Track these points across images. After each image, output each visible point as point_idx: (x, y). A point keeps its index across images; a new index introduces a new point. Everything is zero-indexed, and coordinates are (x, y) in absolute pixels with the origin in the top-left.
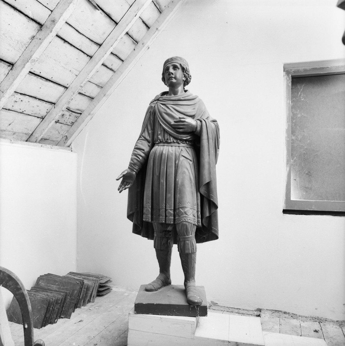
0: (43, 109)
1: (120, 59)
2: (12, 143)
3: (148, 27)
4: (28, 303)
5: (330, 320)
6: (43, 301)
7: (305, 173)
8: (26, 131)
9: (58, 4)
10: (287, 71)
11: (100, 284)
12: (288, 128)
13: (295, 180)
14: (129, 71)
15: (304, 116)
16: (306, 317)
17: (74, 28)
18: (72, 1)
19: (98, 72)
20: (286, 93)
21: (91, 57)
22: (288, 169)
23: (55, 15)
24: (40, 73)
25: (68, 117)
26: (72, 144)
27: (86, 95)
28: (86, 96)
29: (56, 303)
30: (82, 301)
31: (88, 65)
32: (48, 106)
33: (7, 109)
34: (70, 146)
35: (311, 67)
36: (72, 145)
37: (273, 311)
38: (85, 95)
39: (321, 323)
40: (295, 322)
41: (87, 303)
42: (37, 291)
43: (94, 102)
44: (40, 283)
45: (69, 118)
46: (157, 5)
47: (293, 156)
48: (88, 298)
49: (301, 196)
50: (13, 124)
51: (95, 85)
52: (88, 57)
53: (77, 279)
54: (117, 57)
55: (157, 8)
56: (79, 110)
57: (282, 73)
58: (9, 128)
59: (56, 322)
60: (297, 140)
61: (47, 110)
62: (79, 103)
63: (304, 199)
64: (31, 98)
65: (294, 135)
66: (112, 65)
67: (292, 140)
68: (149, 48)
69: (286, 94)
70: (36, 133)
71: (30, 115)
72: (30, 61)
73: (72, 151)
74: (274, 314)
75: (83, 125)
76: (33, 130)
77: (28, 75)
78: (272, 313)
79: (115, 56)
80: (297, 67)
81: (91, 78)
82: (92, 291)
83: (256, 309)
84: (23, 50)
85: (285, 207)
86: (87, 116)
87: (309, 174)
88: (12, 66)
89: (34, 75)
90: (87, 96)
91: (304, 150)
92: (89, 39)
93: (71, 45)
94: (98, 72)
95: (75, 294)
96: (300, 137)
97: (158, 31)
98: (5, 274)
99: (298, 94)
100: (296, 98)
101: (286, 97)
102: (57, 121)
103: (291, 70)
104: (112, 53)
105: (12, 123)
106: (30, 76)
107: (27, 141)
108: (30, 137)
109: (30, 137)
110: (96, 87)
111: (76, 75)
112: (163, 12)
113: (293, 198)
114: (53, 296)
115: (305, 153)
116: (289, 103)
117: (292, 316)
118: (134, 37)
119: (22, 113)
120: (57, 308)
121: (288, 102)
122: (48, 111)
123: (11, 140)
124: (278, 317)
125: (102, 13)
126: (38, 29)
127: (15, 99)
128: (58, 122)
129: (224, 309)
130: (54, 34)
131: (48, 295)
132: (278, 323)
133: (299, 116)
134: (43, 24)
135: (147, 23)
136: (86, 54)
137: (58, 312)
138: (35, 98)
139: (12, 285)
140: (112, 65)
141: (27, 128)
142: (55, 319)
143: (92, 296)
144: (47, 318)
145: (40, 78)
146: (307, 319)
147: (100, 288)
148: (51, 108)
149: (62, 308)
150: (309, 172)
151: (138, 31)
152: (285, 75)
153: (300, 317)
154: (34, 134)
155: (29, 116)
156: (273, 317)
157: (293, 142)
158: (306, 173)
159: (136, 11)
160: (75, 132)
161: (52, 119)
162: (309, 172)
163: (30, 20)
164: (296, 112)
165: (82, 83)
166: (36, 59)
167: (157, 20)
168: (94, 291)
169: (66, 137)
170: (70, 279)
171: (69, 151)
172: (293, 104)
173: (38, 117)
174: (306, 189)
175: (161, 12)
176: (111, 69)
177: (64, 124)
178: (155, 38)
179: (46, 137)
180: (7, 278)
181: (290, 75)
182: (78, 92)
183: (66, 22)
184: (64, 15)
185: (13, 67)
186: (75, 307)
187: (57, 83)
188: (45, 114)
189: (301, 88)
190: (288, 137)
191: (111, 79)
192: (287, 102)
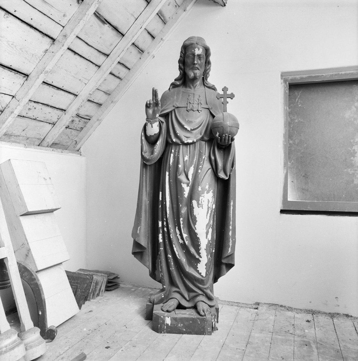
0: (54, 115)
1: (126, 67)
2: (26, 147)
3: (153, 37)
5: (323, 313)
7: (301, 175)
9: (69, 20)
10: (285, 79)
11: (108, 280)
12: (285, 133)
13: (293, 182)
16: (301, 310)
17: (84, 41)
18: (82, 18)
20: (284, 100)
21: (99, 67)
22: (285, 172)
23: (67, 30)
24: (52, 82)
25: (77, 122)
27: (95, 101)
28: (94, 102)
30: (92, 294)
32: (59, 112)
33: (21, 116)
34: (79, 150)
37: (270, 305)
40: (289, 314)
41: (96, 296)
43: (102, 108)
45: (78, 123)
46: (162, 17)
47: (291, 159)
48: (97, 292)
49: (298, 197)
50: (27, 129)
51: (103, 93)
53: (86, 274)
54: (124, 65)
55: (162, 19)
58: (23, 134)
62: (88, 110)
63: (301, 200)
64: (43, 106)
65: (292, 140)
66: (119, 73)
67: (290, 144)
69: (283, 101)
70: (47, 138)
71: (42, 121)
72: (43, 72)
74: (271, 307)
76: (44, 136)
77: (42, 85)
79: (122, 65)
81: (100, 86)
82: (101, 286)
83: (254, 303)
84: (37, 62)
87: (306, 176)
88: (27, 77)
90: (95, 103)
91: (301, 154)
92: (97, 50)
93: (81, 56)
95: (85, 287)
96: (297, 141)
97: (163, 41)
98: (21, 266)
100: (293, 104)
102: (67, 127)
104: (119, 62)
105: (26, 128)
107: (39, 145)
108: (42, 142)
109: (42, 142)
112: (167, 23)
116: (287, 109)
118: (140, 47)
121: (286, 108)
122: (59, 117)
123: (25, 145)
125: (110, 26)
126: (51, 44)
127: (29, 107)
129: (224, 303)
130: (65, 47)
133: (296, 122)
134: (55, 38)
135: (152, 34)
136: (95, 64)
138: (48, 105)
139: (28, 276)
140: (119, 73)
141: (39, 134)
143: (101, 291)
145: (52, 87)
147: (108, 283)
150: (306, 174)
151: (144, 41)
154: (45, 139)
155: (41, 122)
157: (291, 146)
158: (303, 175)
159: (141, 24)
161: (63, 125)
162: (306, 174)
163: (44, 36)
164: (293, 118)
165: (91, 91)
166: (49, 71)
167: (161, 31)
168: (102, 286)
170: (80, 274)
171: (78, 155)
172: (290, 110)
173: (50, 123)
174: (303, 190)
175: (165, 23)
176: (118, 78)
177: (74, 129)
178: (160, 48)
179: (57, 142)
180: (23, 270)
181: (288, 83)
182: (87, 99)
183: (77, 37)
184: (75, 30)
185: (28, 77)
186: (85, 300)
187: (67, 91)
189: (298, 93)
192: (285, 108)
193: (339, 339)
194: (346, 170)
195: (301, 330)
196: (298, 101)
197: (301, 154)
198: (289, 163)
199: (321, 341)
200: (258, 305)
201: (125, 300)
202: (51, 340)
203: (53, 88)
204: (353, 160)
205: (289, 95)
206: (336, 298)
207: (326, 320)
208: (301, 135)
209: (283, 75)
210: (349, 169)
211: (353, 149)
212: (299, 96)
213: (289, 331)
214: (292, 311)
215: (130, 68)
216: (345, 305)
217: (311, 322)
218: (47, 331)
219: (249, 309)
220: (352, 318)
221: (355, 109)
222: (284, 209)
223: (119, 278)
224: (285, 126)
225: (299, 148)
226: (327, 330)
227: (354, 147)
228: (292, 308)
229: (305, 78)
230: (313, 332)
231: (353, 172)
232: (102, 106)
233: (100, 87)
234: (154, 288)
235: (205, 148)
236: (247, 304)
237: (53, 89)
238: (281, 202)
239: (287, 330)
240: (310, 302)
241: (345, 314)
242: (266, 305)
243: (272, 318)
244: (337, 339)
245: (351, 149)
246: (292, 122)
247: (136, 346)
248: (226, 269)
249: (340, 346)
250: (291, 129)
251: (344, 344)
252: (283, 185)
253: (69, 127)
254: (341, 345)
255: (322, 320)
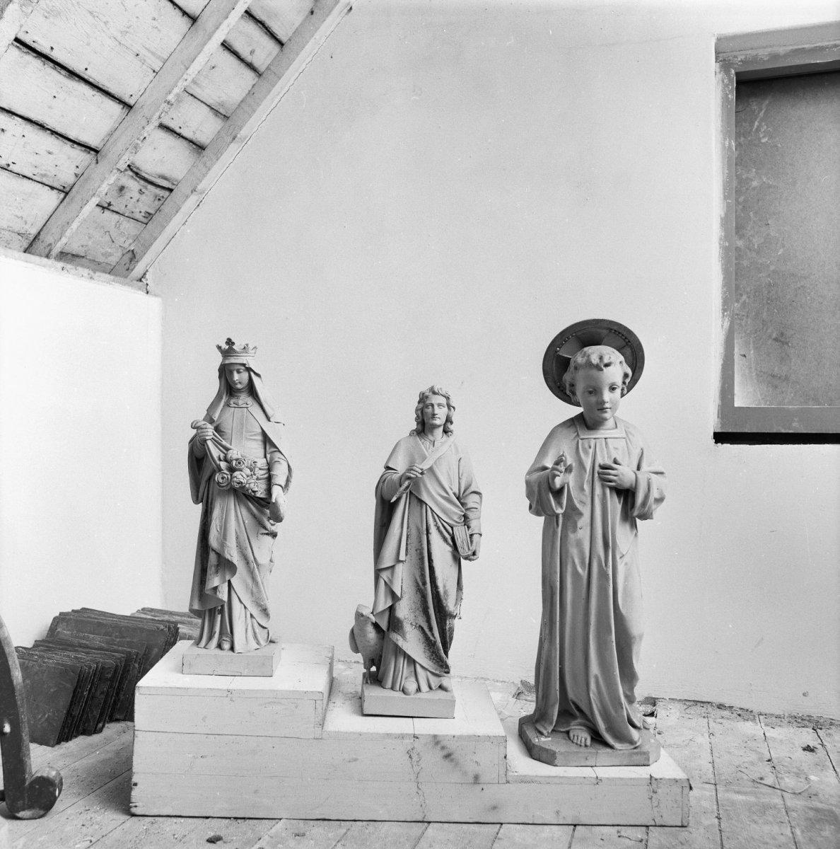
1: (273, 36)
4: (10, 663)
6: (64, 671)
7: (770, 336)
8: (18, 226)
10: (724, 60)
13: (745, 356)
14: (297, 74)
15: (769, 184)
19: (213, 67)
20: (722, 121)
22: (727, 324)
24: (52, 48)
25: (136, 195)
26: (148, 273)
29: (100, 679)
31: (185, 41)
35: (791, 48)
36: (147, 276)
38: (179, 135)
39: (818, 730)
40: (748, 728)
42: (49, 649)
43: (205, 157)
44: (59, 630)
45: (139, 199)
51: (208, 109)
52: (186, 19)
53: (158, 620)
54: (266, 28)
56: (166, 178)
57: (713, 65)
59: (101, 731)
60: (750, 250)
61: (77, 167)
65: (741, 237)
66: (252, 52)
67: (738, 249)
68: (351, 8)
70: (48, 233)
71: (29, 179)
73: (147, 293)
75: (178, 219)
78: (685, 707)
79: (261, 26)
80: (752, 49)
85: (720, 426)
86: (187, 197)
89: (35, 55)
94: (213, 67)
95: (153, 656)
96: (756, 241)
99: (753, 126)
100: (745, 137)
101: (722, 132)
102: (106, 205)
103: (735, 57)
106: (23, 55)
110: (211, 115)
111: (154, 71)
113: (738, 403)
114: (88, 660)
115: (770, 285)
117: (739, 715)
119: (6, 169)
120: (102, 693)
122: (79, 171)
124: (704, 717)
128: (109, 209)
131: (76, 658)
132: (704, 730)
136: (180, 8)
137: (105, 702)
138: (42, 127)
140: (252, 52)
142: (99, 722)
144: (74, 717)
145: (52, 65)
146: (781, 721)
148: (86, 164)
149: (118, 694)
150: (782, 334)
152: (718, 70)
153: (761, 717)
155: (25, 181)
156: (690, 716)
158: (774, 336)
160: (155, 239)
165: (170, 92)
169: (130, 253)
173: (52, 188)
174: (772, 380)
176: (250, 66)
179: (75, 248)
181: (733, 72)
188: (71, 180)
189: (761, 107)
190: (726, 237)
191: (251, 93)
195: (797, 775)
196: (758, 127)
200: (654, 705)
202: (42, 812)
203: (55, 69)
205: (736, 112)
208: (769, 222)
212: (761, 114)
213: (761, 779)
214: (754, 720)
218: (32, 783)
222: (724, 431)
224: (725, 197)
229: (786, 56)
232: (205, 153)
233: (194, 86)
235: (406, 500)
237: (54, 73)
239: (756, 776)
242: (678, 705)
243: (703, 740)
246: (741, 187)
247: (304, 835)
250: (741, 207)
252: (721, 362)
253: (111, 208)
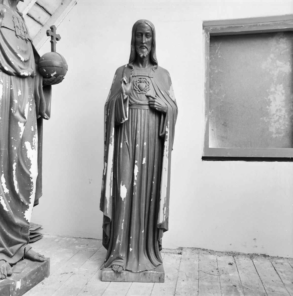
13: (213, 130)
16: (222, 252)
22: (206, 120)
40: (212, 257)
54: (45, 9)
65: (212, 89)
66: (39, 18)
67: (210, 93)
83: (178, 248)
87: (225, 125)
100: (213, 55)
140: (39, 18)
150: (225, 123)
158: (222, 123)
162: (225, 123)
174: (222, 138)
181: (209, 33)
193: (262, 281)
194: (262, 118)
196: (218, 52)
197: (221, 103)
198: (210, 112)
199: (246, 285)
201: (47, 252)
204: (268, 109)
206: (254, 239)
207: (247, 261)
209: (206, 26)
210: (264, 117)
211: (269, 98)
212: (218, 48)
215: (52, 14)
216: (263, 246)
217: (233, 264)
219: (173, 255)
220: (270, 258)
221: (270, 60)
222: (205, 156)
223: (42, 229)
225: (219, 97)
226: (249, 272)
227: (269, 96)
228: (214, 251)
230: (237, 275)
231: (268, 120)
234: (79, 238)
236: (170, 249)
238: (203, 150)
240: (230, 245)
241: (263, 254)
242: (189, 250)
244: (261, 282)
245: (266, 99)
246: (212, 72)
248: (44, 93)
249: (265, 289)
250: (212, 79)
251: (268, 286)
254: (266, 288)
255: (244, 262)
